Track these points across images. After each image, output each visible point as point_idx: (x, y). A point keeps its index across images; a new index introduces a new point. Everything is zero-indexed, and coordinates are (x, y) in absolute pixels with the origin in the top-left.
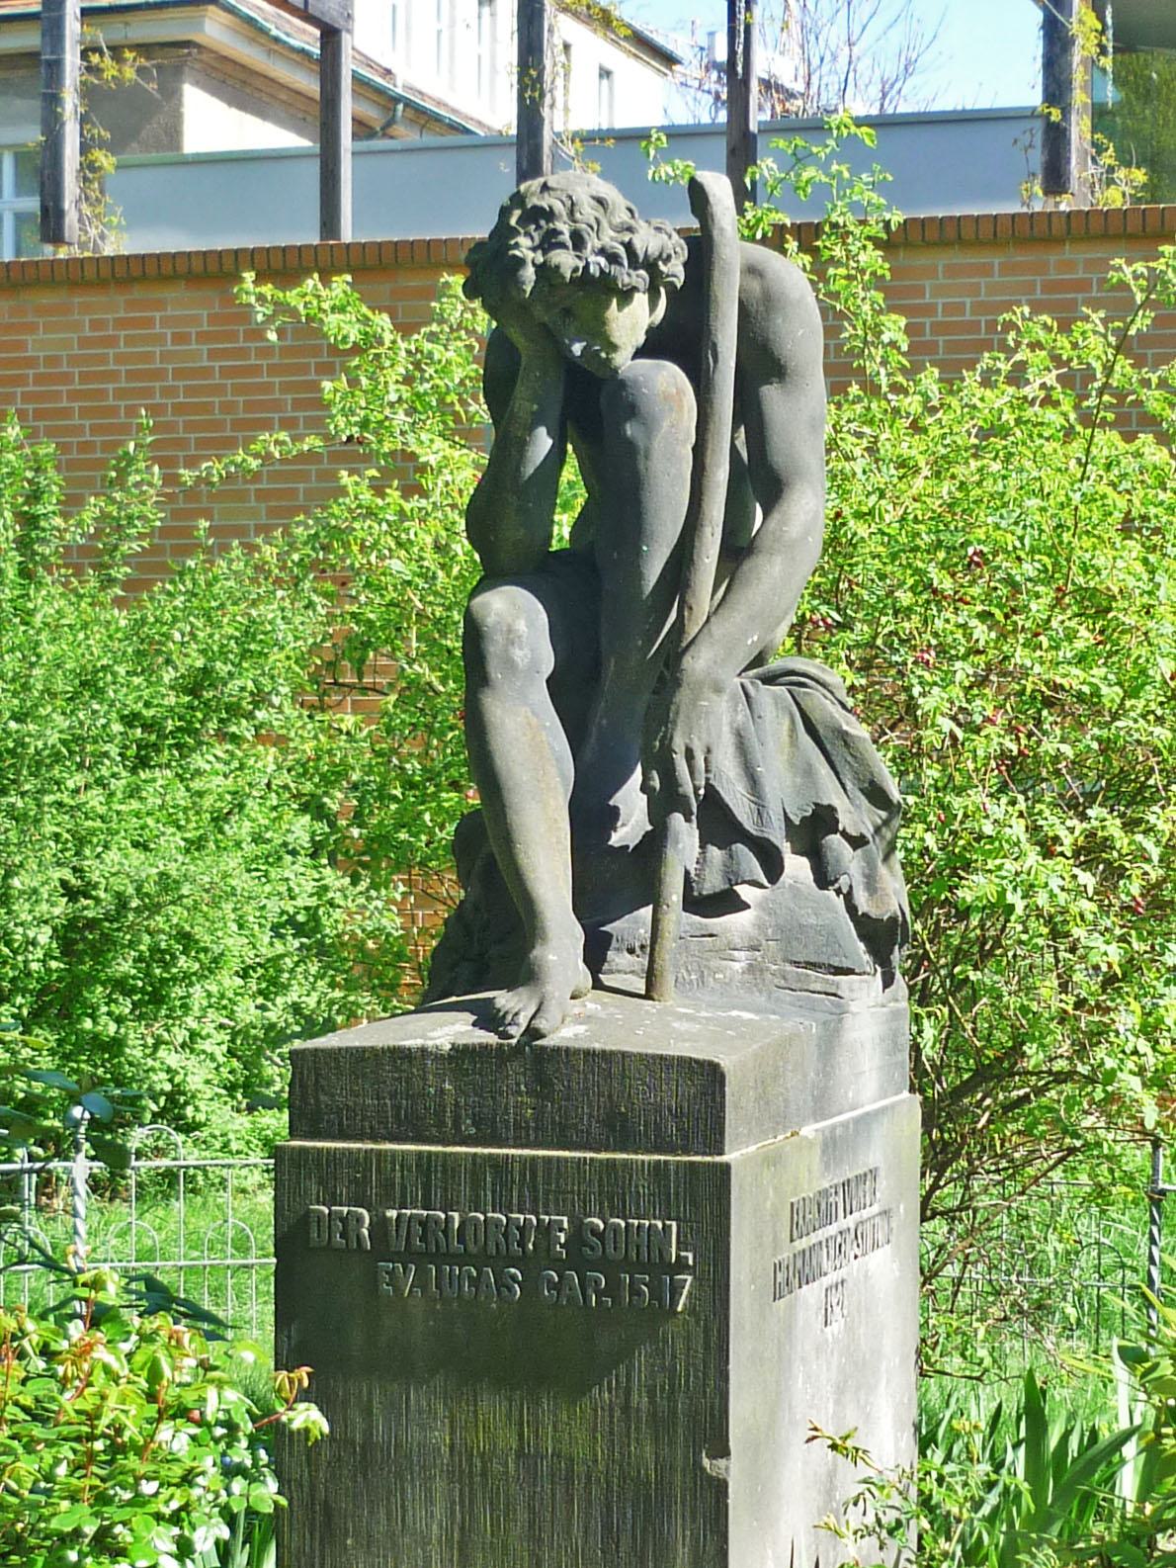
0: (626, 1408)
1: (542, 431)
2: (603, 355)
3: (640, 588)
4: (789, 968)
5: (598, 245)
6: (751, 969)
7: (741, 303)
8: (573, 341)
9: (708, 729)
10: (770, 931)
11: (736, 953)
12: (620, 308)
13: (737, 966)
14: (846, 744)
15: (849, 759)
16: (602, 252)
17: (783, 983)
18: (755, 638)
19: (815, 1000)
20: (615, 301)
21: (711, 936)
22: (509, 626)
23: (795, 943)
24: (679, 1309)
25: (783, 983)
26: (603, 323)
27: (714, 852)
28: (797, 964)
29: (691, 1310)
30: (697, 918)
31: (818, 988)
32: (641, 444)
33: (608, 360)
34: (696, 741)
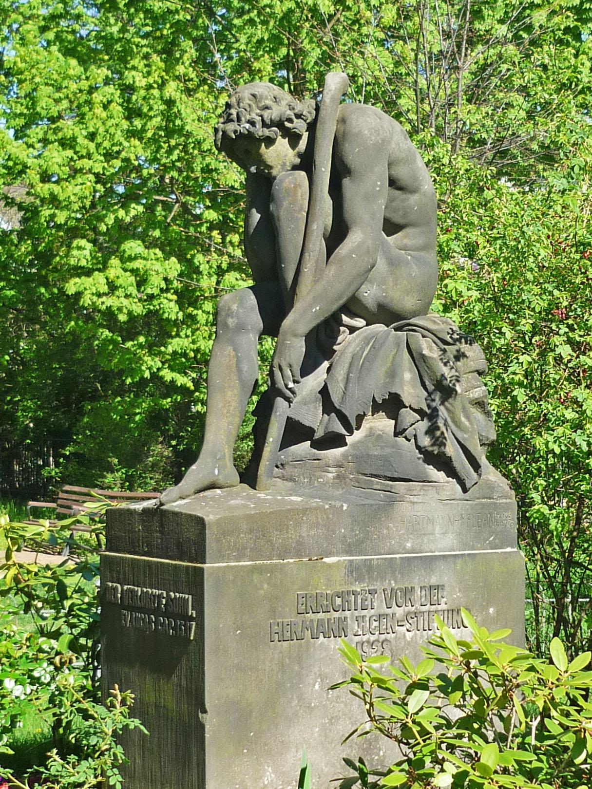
0: (180, 685)
1: (254, 210)
2: (266, 171)
3: (286, 286)
4: (361, 477)
5: (248, 117)
6: (338, 477)
7: (335, 136)
8: (251, 166)
9: (290, 356)
10: (350, 458)
11: (330, 469)
12: (267, 147)
13: (331, 475)
14: (424, 362)
15: (426, 368)
16: (249, 122)
17: (357, 485)
18: (318, 308)
19: (376, 494)
20: (263, 144)
21: (318, 460)
22: (229, 307)
23: (364, 464)
24: (192, 638)
25: (357, 485)
26: (260, 156)
27: (325, 415)
28: (365, 475)
29: (195, 639)
30: (316, 451)
31: (379, 487)
32: (275, 214)
33: (270, 173)
34: (283, 362)
